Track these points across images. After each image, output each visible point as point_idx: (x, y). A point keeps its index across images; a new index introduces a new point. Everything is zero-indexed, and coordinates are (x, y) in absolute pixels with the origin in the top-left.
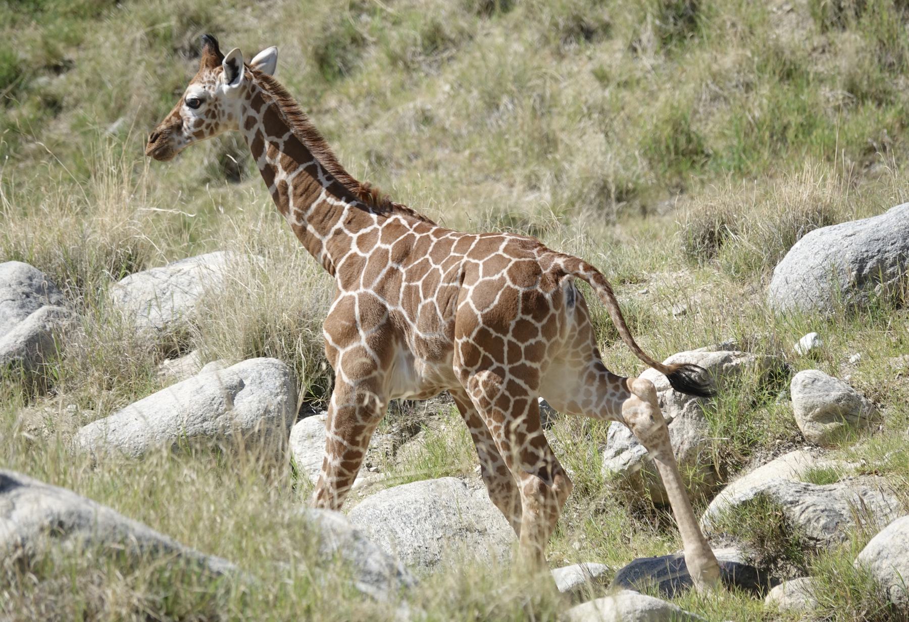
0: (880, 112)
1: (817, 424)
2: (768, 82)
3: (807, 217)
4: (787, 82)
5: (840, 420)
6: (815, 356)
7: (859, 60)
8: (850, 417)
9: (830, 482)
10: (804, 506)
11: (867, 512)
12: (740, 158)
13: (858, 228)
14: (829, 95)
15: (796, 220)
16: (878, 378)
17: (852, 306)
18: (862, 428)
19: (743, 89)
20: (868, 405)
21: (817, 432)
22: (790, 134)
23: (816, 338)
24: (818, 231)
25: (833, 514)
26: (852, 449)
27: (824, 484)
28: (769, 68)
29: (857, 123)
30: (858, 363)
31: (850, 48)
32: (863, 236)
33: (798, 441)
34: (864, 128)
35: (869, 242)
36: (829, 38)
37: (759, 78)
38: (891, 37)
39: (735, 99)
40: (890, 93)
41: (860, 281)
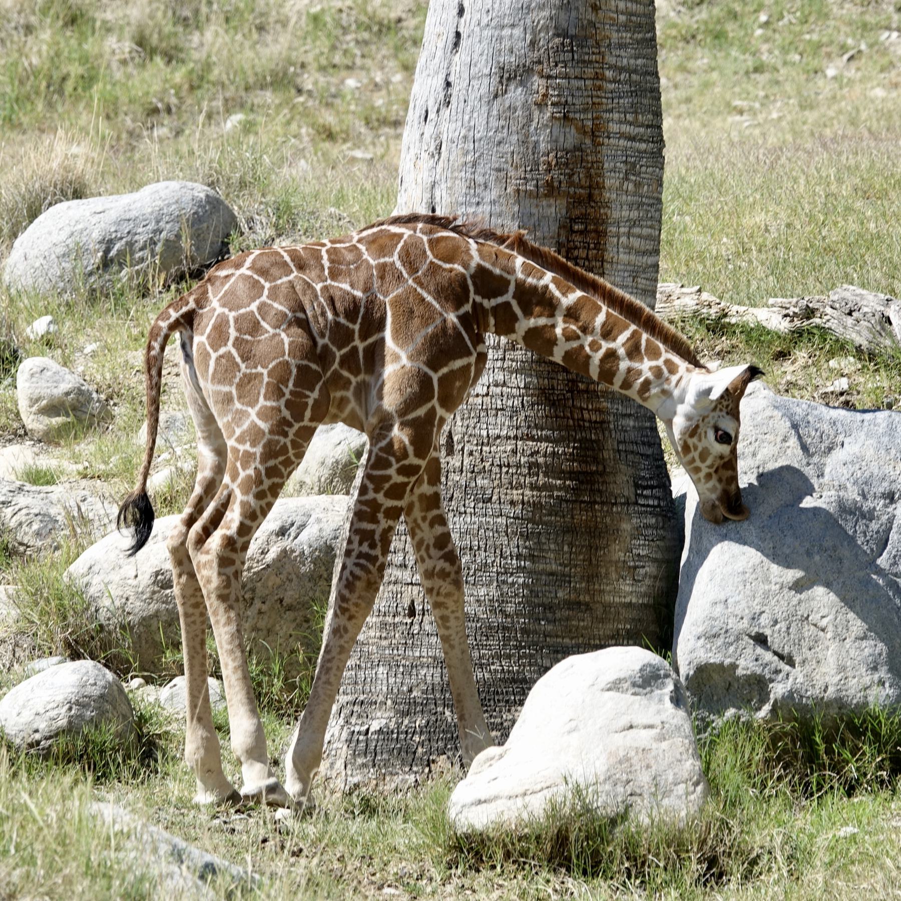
0: (169, 70)
1: (42, 418)
2: (51, 27)
3: (55, 187)
4: (70, 28)
5: (68, 415)
6: (48, 342)
8: (79, 414)
9: (48, 483)
10: (17, 508)
11: (85, 521)
12: (12, 107)
13: (108, 206)
14: (115, 46)
15: (43, 190)
16: (114, 373)
17: (94, 290)
19: (22, 31)
20: (99, 401)
21: (41, 427)
22: (69, 86)
23: (51, 322)
24: (64, 205)
25: (47, 519)
26: (77, 448)
27: (42, 485)
28: (52, 12)
29: (143, 81)
30: (94, 354)
32: (112, 215)
33: (21, 434)
34: (149, 86)
35: (118, 222)
37: (41, 21)
39: (12, 42)
40: (181, 50)
41: (106, 263)
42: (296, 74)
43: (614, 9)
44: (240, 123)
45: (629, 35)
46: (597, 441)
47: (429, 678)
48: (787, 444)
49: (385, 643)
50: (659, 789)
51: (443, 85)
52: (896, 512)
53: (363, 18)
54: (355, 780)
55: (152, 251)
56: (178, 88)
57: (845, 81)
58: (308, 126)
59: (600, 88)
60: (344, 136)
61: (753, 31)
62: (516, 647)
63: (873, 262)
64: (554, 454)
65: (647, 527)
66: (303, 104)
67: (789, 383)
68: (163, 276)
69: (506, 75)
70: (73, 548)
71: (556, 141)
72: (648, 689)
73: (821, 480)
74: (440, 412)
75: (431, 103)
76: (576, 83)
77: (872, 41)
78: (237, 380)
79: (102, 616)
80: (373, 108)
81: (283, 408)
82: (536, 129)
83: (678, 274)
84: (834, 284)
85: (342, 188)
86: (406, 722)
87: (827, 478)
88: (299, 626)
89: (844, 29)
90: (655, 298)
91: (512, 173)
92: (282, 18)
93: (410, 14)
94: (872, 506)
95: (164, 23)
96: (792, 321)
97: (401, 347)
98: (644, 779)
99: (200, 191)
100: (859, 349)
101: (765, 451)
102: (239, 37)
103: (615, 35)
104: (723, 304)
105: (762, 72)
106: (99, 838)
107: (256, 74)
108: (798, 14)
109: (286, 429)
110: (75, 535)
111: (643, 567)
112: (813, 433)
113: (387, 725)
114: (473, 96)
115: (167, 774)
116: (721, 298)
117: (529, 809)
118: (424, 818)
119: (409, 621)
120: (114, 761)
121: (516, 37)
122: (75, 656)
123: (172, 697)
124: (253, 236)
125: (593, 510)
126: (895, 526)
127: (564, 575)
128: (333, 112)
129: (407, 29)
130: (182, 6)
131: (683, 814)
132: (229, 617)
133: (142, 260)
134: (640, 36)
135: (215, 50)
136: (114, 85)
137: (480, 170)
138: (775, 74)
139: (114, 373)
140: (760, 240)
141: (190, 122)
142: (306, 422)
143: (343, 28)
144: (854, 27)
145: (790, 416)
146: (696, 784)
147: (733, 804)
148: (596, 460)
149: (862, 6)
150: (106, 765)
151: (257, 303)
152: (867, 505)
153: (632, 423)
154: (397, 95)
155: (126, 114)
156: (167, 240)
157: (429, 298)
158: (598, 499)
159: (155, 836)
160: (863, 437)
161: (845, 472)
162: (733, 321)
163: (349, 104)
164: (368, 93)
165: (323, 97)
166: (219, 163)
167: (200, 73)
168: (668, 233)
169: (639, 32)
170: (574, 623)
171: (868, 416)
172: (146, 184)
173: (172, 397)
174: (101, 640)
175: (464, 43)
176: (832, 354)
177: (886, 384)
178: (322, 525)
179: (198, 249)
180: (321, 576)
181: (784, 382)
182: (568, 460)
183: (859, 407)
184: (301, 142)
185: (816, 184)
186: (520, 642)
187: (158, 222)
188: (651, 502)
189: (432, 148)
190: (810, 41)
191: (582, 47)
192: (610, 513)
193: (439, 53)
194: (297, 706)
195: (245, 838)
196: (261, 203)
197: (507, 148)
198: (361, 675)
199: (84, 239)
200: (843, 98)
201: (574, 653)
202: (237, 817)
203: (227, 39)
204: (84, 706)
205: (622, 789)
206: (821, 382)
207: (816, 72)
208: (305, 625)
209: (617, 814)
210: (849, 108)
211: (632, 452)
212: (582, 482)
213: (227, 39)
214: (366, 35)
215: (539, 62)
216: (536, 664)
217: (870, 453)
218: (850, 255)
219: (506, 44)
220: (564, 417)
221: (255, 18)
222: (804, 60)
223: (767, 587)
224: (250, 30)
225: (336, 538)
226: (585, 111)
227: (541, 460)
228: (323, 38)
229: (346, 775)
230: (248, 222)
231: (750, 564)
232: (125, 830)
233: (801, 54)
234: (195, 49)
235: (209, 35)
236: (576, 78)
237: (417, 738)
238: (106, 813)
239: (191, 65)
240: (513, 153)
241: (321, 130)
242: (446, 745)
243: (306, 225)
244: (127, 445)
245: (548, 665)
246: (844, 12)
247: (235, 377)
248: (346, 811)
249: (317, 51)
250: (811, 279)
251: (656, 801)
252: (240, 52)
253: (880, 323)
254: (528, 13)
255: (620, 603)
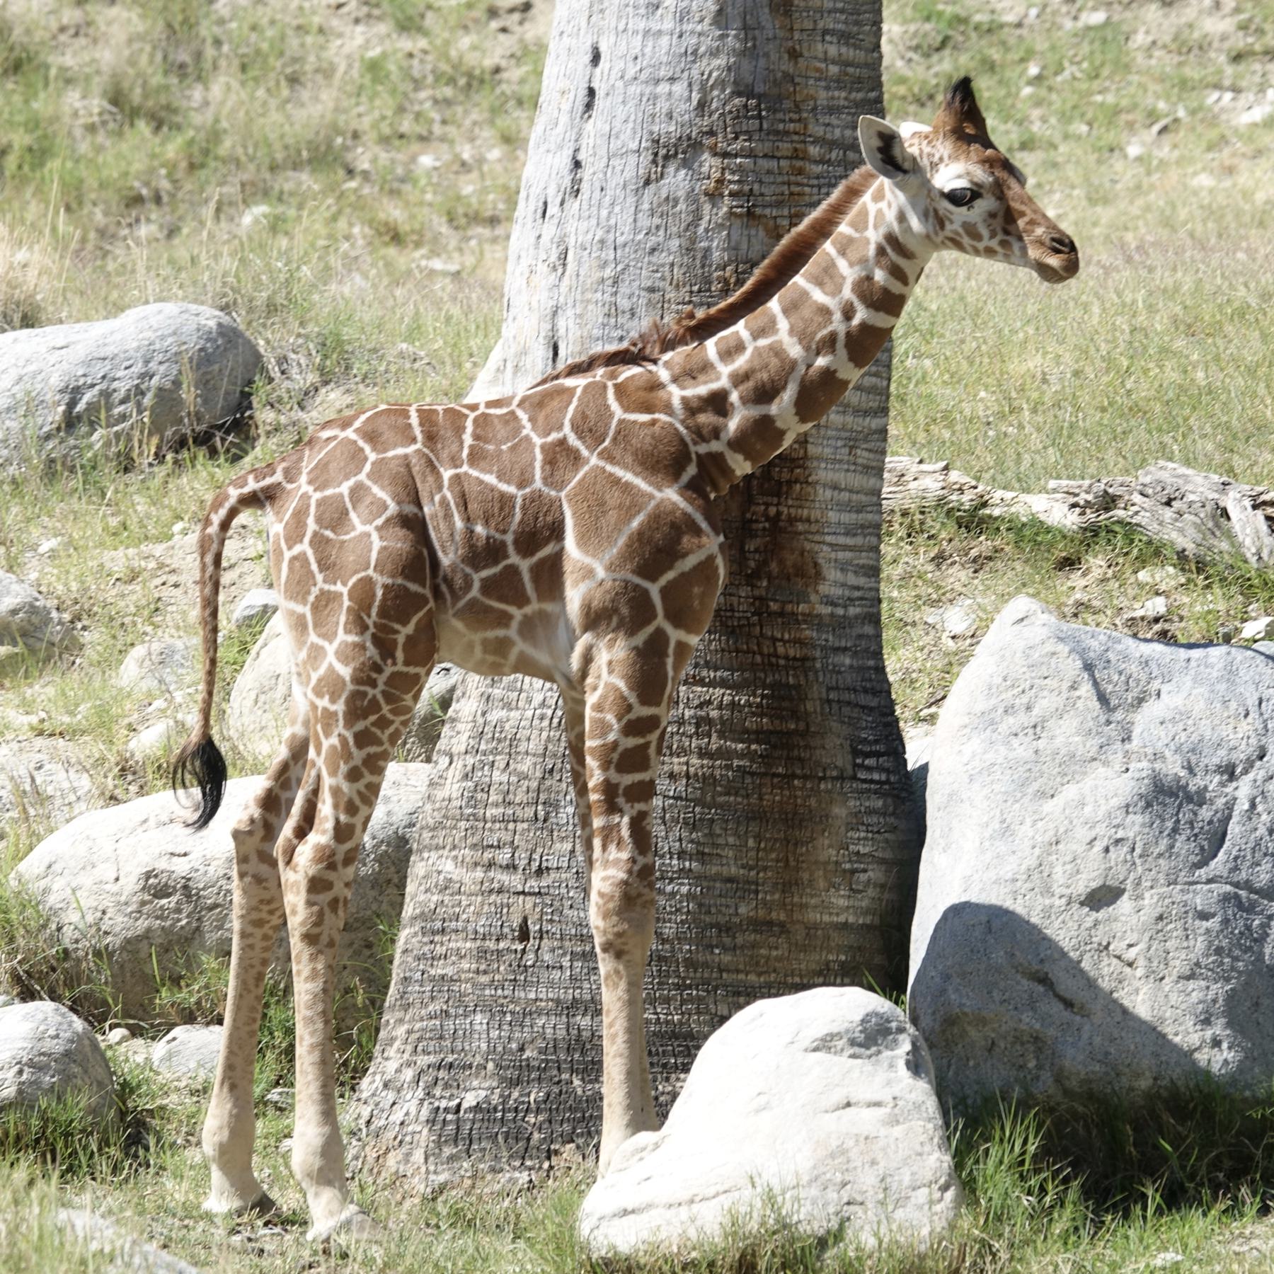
0: (157, 140)
4: (13, 79)
5: (15, 644)
7: (132, 55)
8: (31, 641)
11: (41, 798)
14: (78, 105)
16: (83, 582)
17: (53, 461)
18: (47, 659)
20: (60, 623)
26: (29, 692)
29: (119, 156)
30: (53, 555)
31: (118, 35)
32: (80, 352)
34: (129, 164)
35: (89, 362)
36: (87, 13)
38: (185, 21)
40: (175, 111)
41: (70, 422)
42: (345, 148)
43: (821, 55)
44: (265, 216)
45: (843, 94)
46: (797, 687)
47: (549, 1031)
48: (1077, 693)
49: (484, 979)
50: (889, 1197)
51: (570, 165)
52: (1237, 794)
53: (444, 67)
54: (442, 1178)
55: (139, 404)
56: (172, 167)
57: (1155, 163)
58: (363, 224)
59: (800, 172)
60: (415, 237)
61: (1019, 90)
62: (677, 986)
63: (1201, 428)
64: (733, 705)
65: (871, 812)
66: (356, 190)
67: (1079, 604)
68: (155, 440)
69: (663, 152)
70: (23, 838)
71: (736, 249)
72: (874, 1049)
73: (1127, 746)
74: (675, 635)
75: (551, 191)
76: (765, 164)
77: (1195, 104)
78: (311, 598)
79: (68, 934)
80: (459, 198)
81: (369, 644)
82: (707, 230)
83: (914, 443)
84: (1144, 460)
85: (417, 313)
86: (515, 1094)
87: (1135, 743)
88: (357, 953)
89: (1153, 87)
90: (881, 478)
91: (671, 295)
92: (325, 65)
93: (513, 61)
94: (1202, 784)
95: (150, 71)
96: (1083, 514)
97: (594, 556)
98: (867, 1181)
99: (209, 317)
100: (1181, 555)
101: (1044, 703)
102: (261, 93)
103: (823, 94)
104: (980, 488)
105: (1032, 150)
106: (69, 1261)
107: (286, 147)
108: (1085, 65)
109: (374, 675)
110: (27, 819)
111: (865, 871)
112: (1116, 677)
113: (487, 1100)
114: (615, 181)
115: (163, 1168)
116: (978, 479)
117: (698, 1223)
118: (543, 1235)
119: (520, 947)
120: (85, 1148)
121: (676, 96)
122: (27, 995)
123: (169, 1056)
124: (287, 384)
125: (791, 787)
126: (1235, 813)
127: (748, 882)
128: (400, 204)
129: (508, 82)
130: (177, 47)
131: (925, 1231)
132: (314, 969)
133: (123, 417)
134: (860, 96)
135: (225, 111)
136: (77, 161)
137: (624, 289)
138: (1052, 153)
139: (83, 582)
140: (1035, 395)
141: (189, 218)
142: (400, 667)
143: (415, 81)
144: (1168, 84)
145: (1082, 652)
146: (945, 1188)
147: (999, 1218)
148: (795, 715)
149: (1180, 53)
150: (74, 1154)
151: (351, 482)
152: (1195, 784)
153: (848, 661)
154: (494, 179)
155: (95, 204)
156: (160, 389)
157: (627, 476)
158: (798, 772)
159: (151, 1259)
160: (1189, 684)
161: (1163, 735)
162: (996, 512)
163: (423, 192)
164: (451, 176)
165: (385, 181)
166: (237, 276)
167: (204, 145)
168: (900, 384)
169: (859, 90)
170: (763, 951)
171: (1196, 653)
172: (129, 307)
173: (168, 617)
174: (65, 971)
175: (599, 102)
176: (1141, 562)
177: (1222, 606)
178: (390, 806)
179: (206, 402)
180: (389, 881)
181: (1071, 602)
182: (754, 714)
183: (1182, 640)
184: (353, 246)
185: (1116, 314)
186: (684, 979)
187: (147, 362)
188: (876, 776)
189: (553, 257)
190: (1102, 104)
191: (775, 111)
192: (815, 791)
193: (564, 119)
194: (355, 1070)
195: (279, 1262)
196: (299, 335)
197: (663, 258)
198: (450, 1025)
199: (39, 386)
200: (1152, 187)
201: (763, 997)
202: (267, 1231)
203: (244, 95)
204: (40, 1069)
205: (835, 1195)
206: (1126, 603)
207: (1112, 150)
208: (367, 952)
209: (828, 1232)
210: (1161, 203)
211: (849, 703)
212: (774, 747)
213: (244, 95)
214: (448, 92)
215: (711, 133)
216: (707, 1012)
217: (1199, 707)
218: (1169, 417)
219: (662, 106)
220: (748, 652)
221: (284, 66)
222: (1094, 132)
223: (1047, 902)
224: (278, 83)
225: (412, 825)
226: (779, 204)
227: (714, 714)
228: (385, 95)
229: (428, 1172)
230: (279, 363)
231: (1024, 867)
232: (107, 1250)
233: (1090, 124)
234: (196, 110)
235: (216, 90)
236: (765, 156)
237: (531, 1119)
238: (79, 1224)
239: (191, 133)
240: (672, 265)
241: (382, 229)
242: (574, 1129)
243: (365, 368)
244: (103, 689)
245: (725, 1013)
246: (1153, 62)
247: (308, 593)
248: (428, 1225)
249: (377, 114)
250: (1111, 452)
251: (885, 1212)
252: (263, 115)
253: (1213, 517)
254: (694, 62)
255: (831, 923)
